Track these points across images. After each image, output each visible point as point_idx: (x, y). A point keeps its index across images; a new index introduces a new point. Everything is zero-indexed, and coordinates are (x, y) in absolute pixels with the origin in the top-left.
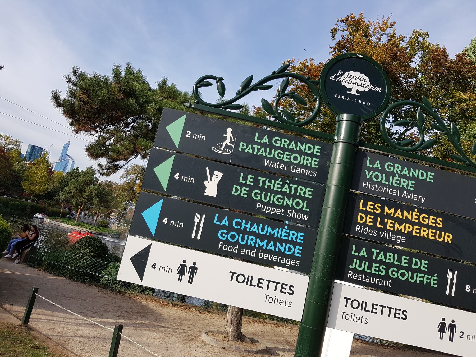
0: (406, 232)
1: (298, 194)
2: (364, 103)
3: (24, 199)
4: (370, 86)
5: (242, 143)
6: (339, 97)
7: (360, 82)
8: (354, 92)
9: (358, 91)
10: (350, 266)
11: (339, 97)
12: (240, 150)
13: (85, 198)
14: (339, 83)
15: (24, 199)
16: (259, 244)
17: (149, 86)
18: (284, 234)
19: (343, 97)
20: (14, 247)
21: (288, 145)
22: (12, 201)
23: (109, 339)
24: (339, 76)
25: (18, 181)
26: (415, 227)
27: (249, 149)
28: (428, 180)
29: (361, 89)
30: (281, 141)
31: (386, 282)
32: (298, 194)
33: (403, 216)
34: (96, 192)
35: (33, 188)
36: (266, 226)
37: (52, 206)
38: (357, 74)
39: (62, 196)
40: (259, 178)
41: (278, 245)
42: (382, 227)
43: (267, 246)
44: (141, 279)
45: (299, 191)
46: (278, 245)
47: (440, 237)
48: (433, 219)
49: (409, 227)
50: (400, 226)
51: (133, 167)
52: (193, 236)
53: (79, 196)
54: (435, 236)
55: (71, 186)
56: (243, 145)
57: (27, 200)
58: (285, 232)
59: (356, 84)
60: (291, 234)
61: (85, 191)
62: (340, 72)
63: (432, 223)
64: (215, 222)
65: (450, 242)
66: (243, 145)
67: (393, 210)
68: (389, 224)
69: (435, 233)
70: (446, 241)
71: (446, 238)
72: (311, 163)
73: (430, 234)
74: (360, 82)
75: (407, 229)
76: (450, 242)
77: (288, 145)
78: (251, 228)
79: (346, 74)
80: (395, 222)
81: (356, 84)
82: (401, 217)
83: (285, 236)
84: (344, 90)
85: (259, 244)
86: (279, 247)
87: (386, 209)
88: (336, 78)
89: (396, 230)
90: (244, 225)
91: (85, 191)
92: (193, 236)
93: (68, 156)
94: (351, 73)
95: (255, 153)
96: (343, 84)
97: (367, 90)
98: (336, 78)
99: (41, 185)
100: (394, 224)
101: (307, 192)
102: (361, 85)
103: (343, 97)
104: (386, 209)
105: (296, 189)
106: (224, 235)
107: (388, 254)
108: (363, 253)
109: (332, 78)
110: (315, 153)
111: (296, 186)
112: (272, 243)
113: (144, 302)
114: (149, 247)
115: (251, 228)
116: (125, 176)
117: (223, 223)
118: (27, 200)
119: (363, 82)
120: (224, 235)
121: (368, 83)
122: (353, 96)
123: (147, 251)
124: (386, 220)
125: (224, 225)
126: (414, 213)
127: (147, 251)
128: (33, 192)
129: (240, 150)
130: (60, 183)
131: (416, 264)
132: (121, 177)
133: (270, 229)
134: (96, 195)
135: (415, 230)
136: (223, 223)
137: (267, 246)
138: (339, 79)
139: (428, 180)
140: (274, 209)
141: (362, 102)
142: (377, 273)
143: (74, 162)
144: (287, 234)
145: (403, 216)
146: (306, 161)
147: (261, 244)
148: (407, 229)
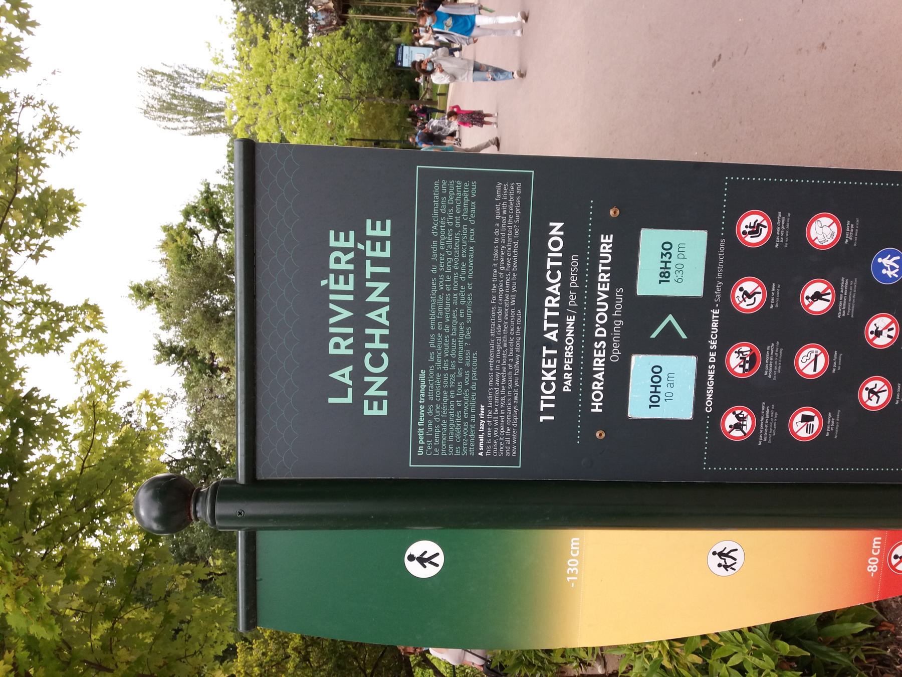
1: (558, 305)
12: (570, 390)
28: (715, 355)
31: (615, 339)
32: (558, 305)
33: (383, 305)
40: (542, 409)
41: (373, 298)
45: (553, 305)
46: (373, 298)
65: (571, 374)
73: (600, 355)
76: (571, 374)
78: (380, 326)
80: (369, 398)
82: (387, 308)
90: (377, 345)
100: (372, 399)
107: (565, 378)
112: (372, 315)
115: (380, 326)
117: (347, 380)
125: (352, 376)
129: (570, 390)
135: (569, 362)
136: (347, 380)
139: (715, 355)
140: (615, 351)
142: (604, 351)
145: (383, 305)
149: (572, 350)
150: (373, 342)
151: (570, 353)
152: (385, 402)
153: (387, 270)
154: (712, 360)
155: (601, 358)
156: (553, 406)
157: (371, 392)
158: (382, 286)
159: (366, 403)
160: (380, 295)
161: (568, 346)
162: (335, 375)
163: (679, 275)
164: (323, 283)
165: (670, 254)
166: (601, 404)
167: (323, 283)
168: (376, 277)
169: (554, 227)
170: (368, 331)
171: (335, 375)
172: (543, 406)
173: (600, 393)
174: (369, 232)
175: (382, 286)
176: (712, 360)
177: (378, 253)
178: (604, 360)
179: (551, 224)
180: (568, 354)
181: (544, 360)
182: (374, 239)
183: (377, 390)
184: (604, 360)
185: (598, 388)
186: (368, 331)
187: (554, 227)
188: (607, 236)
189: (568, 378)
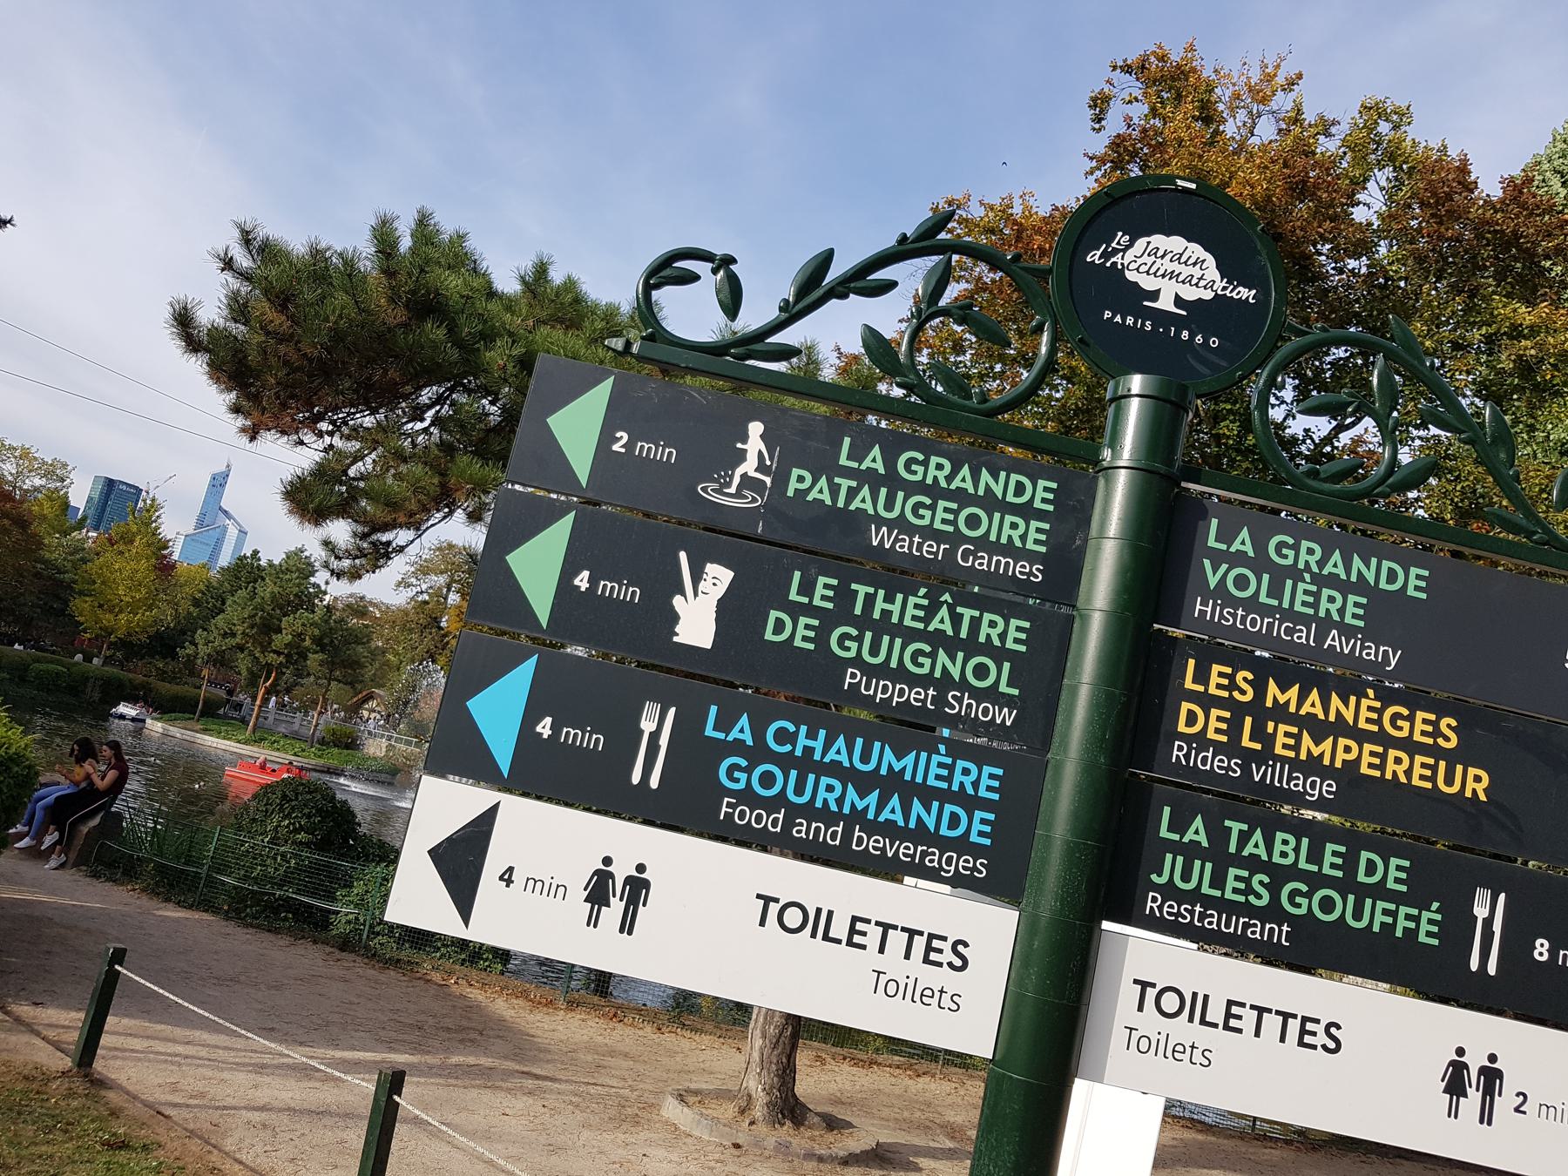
0: (1338, 764)
1: (982, 639)
2: (1199, 339)
3: (79, 657)
4: (1220, 284)
5: (796, 472)
6: (1118, 319)
7: (1186, 271)
8: (1165, 303)
9: (1179, 301)
10: (1154, 877)
11: (1118, 319)
13: (279, 653)
14: (1117, 273)
15: (79, 657)
16: (853, 805)
17: (489, 283)
18: (934, 770)
19: (1130, 321)
20: (45, 815)
21: (949, 479)
22: (38, 661)
23: (359, 1117)
24: (1115, 251)
25: (58, 597)
26: (1368, 747)
27: (821, 491)
29: (1190, 294)
30: (925, 463)
32: (982, 639)
33: (1326, 711)
34: (317, 632)
35: (107, 619)
36: (877, 745)
37: (173, 679)
38: (1176, 243)
39: (203, 645)
40: (854, 586)
41: (917, 807)
43: (879, 811)
45: (985, 629)
46: (917, 807)
47: (1449, 781)
48: (1425, 721)
49: (1347, 749)
50: (1317, 745)
51: (439, 549)
52: (636, 778)
53: (261, 644)
54: (1433, 779)
55: (235, 613)
56: (801, 479)
57: (88, 659)
58: (939, 763)
59: (1172, 275)
60: (958, 770)
61: (279, 631)
62: (1121, 238)
63: (1423, 733)
64: (709, 732)
65: (1483, 797)
66: (801, 479)
67: (1293, 692)
69: (1434, 768)
70: (1468, 794)
71: (1470, 785)
73: (1417, 771)
74: (1186, 271)
75: (1341, 756)
76: (1483, 797)
77: (949, 479)
78: (826, 750)
79: (1141, 243)
80: (1301, 733)
81: (1172, 275)
82: (1321, 716)
83: (938, 777)
84: (1135, 298)
85: (853, 803)
86: (918, 814)
87: (1272, 688)
88: (1106, 255)
90: (802, 741)
91: (279, 631)
92: (636, 778)
93: (225, 512)
94: (1158, 240)
95: (841, 504)
96: (1131, 276)
97: (1208, 295)
98: (1106, 255)
99: (134, 608)
100: (1298, 738)
101: (1012, 634)
102: (1188, 281)
103: (1130, 321)
104: (1272, 688)
105: (975, 624)
106: (737, 774)
107: (1280, 836)
108: (1197, 832)
109: (1094, 257)
110: (1038, 504)
111: (977, 613)
112: (895, 801)
113: (476, 994)
114: (491, 813)
115: (826, 750)
116: (413, 580)
117: (734, 734)
118: (88, 659)
119: (1196, 271)
120: (737, 774)
121: (1212, 273)
122: (1161, 317)
123: (483, 826)
124: (1270, 726)
126: (1365, 703)
127: (483, 826)
128: (109, 632)
130: (196, 603)
131: (1371, 868)
132: (400, 583)
133: (889, 755)
134: (318, 641)
135: (1366, 759)
136: (734, 734)
137: (879, 811)
138: (1117, 259)
141: (1192, 336)
143: (243, 532)
144: (945, 772)
145: (1326, 711)
146: (1009, 529)
147: (860, 805)
148: (1341, 756)
150: (885, 601)
159: (1295, 730)
160: (1338, 711)
166: (895, 619)
170: (822, 733)
172: (862, 590)
183: (868, 806)
186: (822, 733)
188: (1023, 636)
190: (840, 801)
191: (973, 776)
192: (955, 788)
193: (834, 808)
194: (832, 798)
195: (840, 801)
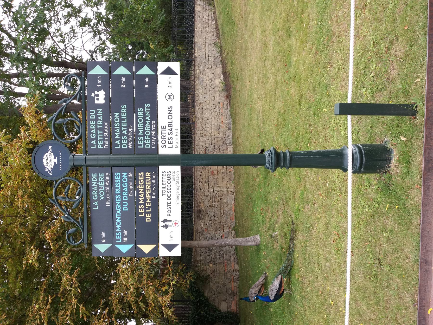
2: (61, 154)
4: (50, 152)
6: (61, 168)
7: (49, 158)
8: (56, 160)
9: (55, 158)
11: (61, 168)
14: (52, 169)
18: (124, 115)
19: (60, 166)
21: (96, 191)
23: (170, 78)
24: (49, 170)
26: (146, 192)
28: (150, 216)
30: (94, 195)
32: (102, 124)
38: (44, 161)
42: (150, 209)
44: (178, 244)
45: (100, 123)
47: (149, 179)
48: (140, 178)
49: (147, 195)
54: (149, 181)
59: (50, 160)
62: (46, 170)
63: (142, 178)
64: (97, 208)
65: (150, 173)
67: (140, 199)
68: (148, 206)
69: (147, 181)
71: (148, 175)
72: (102, 177)
73: (148, 184)
74: (49, 158)
75: (149, 196)
76: (150, 173)
77: (96, 191)
79: (46, 166)
81: (50, 160)
83: (125, 115)
84: (56, 166)
87: (140, 202)
88: (50, 172)
89: (150, 202)
94: (45, 163)
96: (52, 167)
97: (52, 154)
98: (50, 172)
100: (147, 203)
102: (51, 157)
103: (60, 166)
104: (140, 202)
107: (91, 128)
109: (51, 174)
110: (96, 176)
112: (140, 196)
114: (162, 245)
119: (49, 156)
121: (48, 154)
122: (58, 161)
123: (165, 245)
124: (146, 207)
126: (139, 188)
127: (165, 245)
135: (148, 192)
138: (50, 170)
144: (124, 124)
148: (149, 196)
149: (125, 107)
151: (124, 110)
152: (150, 204)
153: (149, 109)
154: (148, 220)
155: (149, 185)
156: (91, 110)
157: (147, 202)
158: (148, 112)
161: (116, 123)
162: (116, 142)
163: (178, 188)
164: (138, 187)
165: (165, 145)
167: (138, 187)
168: (147, 111)
169: (116, 114)
171: (116, 142)
173: (124, 187)
174: (146, 138)
175: (148, 112)
176: (148, 220)
177: (124, 125)
178: (150, 186)
179: (115, 113)
180: (123, 110)
181: (98, 141)
182: (147, 140)
184: (150, 186)
185: (125, 195)
187: (116, 114)
189: (93, 128)
190: (148, 126)
191: (140, 124)
192: (150, 188)
193: (149, 127)
194: (148, 128)
195: (148, 126)
